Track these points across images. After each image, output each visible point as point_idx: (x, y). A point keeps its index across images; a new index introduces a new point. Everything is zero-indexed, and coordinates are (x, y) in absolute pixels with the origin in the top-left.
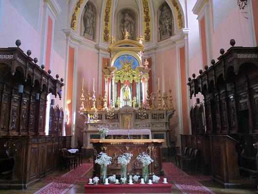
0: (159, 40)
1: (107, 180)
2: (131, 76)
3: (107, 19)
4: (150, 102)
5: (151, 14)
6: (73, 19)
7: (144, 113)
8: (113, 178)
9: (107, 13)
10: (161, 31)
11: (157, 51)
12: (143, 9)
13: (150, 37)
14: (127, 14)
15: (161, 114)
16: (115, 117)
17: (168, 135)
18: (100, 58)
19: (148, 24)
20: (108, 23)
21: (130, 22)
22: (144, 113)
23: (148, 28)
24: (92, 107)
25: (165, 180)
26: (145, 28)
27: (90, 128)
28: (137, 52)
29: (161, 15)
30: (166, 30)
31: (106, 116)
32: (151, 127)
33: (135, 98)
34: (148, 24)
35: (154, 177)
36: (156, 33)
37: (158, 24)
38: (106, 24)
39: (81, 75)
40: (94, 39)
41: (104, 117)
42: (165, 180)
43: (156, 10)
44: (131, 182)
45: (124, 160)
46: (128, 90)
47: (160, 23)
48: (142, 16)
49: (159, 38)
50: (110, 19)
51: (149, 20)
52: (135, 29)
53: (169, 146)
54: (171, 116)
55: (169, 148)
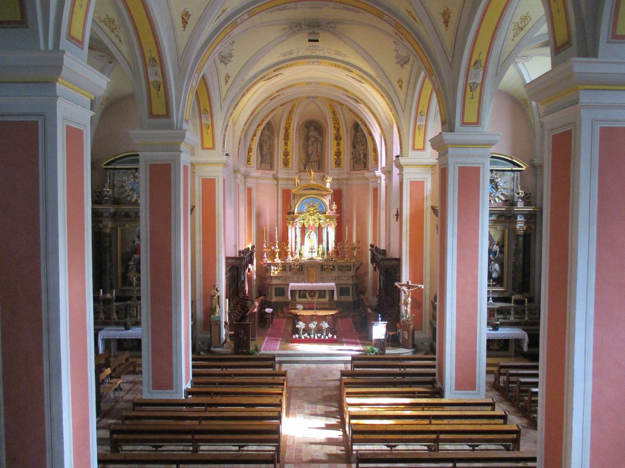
0: (352, 169)
1: (303, 336)
2: (317, 220)
3: (286, 138)
4: (336, 252)
5: (343, 132)
6: (249, 152)
7: (330, 266)
8: (306, 335)
9: (287, 129)
10: (354, 157)
11: (349, 182)
12: (333, 125)
13: (340, 161)
14: (312, 128)
15: (348, 266)
16: (302, 269)
17: (355, 288)
18: (279, 189)
19: (338, 144)
20: (288, 141)
21: (317, 140)
22: (330, 266)
23: (338, 149)
24: (275, 258)
25: (335, 336)
26: (335, 149)
27: (274, 282)
28: (324, 196)
29: (355, 137)
30: (361, 159)
31: (290, 267)
32: (336, 281)
33: (321, 246)
34: (338, 144)
35: (329, 334)
36: (349, 158)
37: (351, 146)
38: (286, 144)
39: (259, 216)
40: (271, 167)
41: (288, 269)
42: (335, 336)
43: (349, 129)
44: (316, 338)
45: (313, 326)
46: (314, 237)
47: (354, 147)
48: (331, 132)
49: (352, 167)
50: (290, 136)
51: (341, 140)
52: (322, 149)
53: (355, 299)
54: (358, 268)
55: (354, 302)
